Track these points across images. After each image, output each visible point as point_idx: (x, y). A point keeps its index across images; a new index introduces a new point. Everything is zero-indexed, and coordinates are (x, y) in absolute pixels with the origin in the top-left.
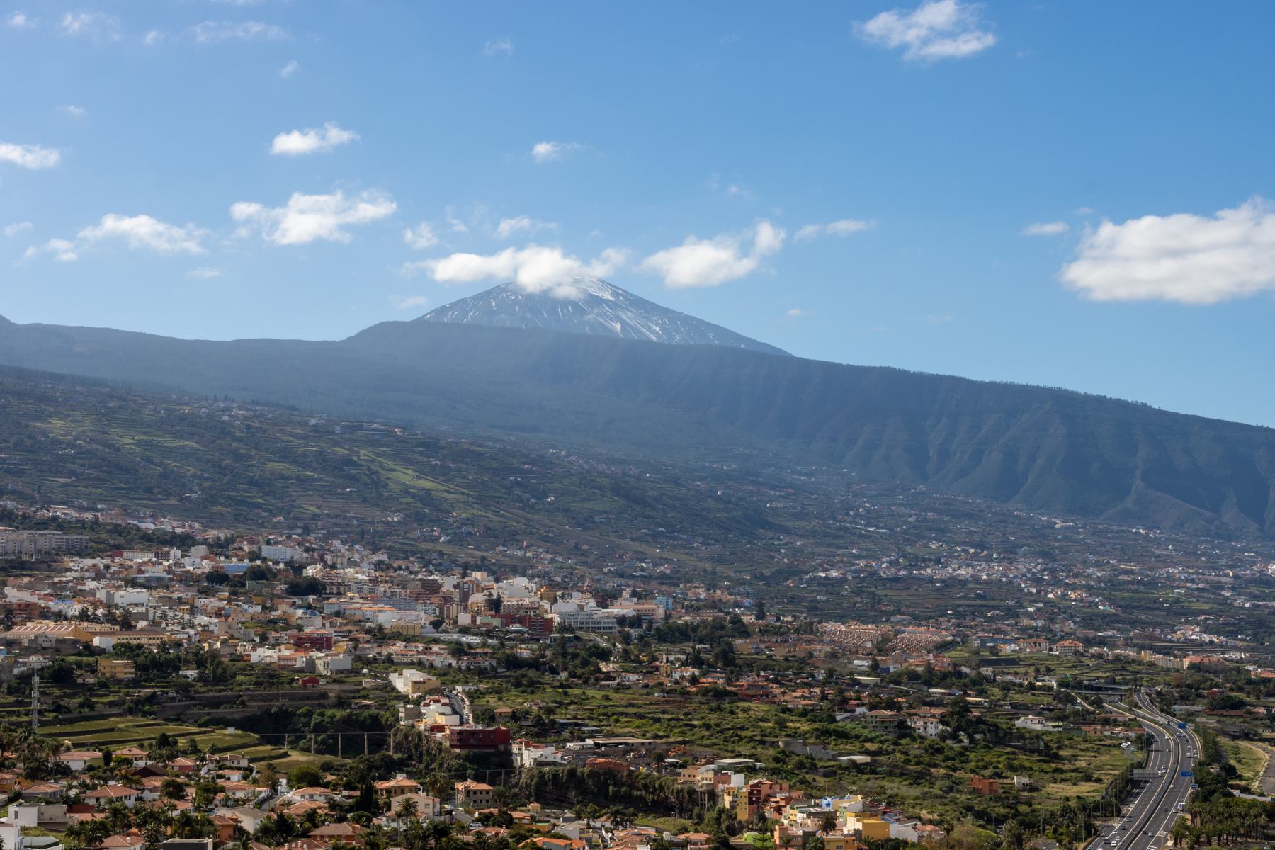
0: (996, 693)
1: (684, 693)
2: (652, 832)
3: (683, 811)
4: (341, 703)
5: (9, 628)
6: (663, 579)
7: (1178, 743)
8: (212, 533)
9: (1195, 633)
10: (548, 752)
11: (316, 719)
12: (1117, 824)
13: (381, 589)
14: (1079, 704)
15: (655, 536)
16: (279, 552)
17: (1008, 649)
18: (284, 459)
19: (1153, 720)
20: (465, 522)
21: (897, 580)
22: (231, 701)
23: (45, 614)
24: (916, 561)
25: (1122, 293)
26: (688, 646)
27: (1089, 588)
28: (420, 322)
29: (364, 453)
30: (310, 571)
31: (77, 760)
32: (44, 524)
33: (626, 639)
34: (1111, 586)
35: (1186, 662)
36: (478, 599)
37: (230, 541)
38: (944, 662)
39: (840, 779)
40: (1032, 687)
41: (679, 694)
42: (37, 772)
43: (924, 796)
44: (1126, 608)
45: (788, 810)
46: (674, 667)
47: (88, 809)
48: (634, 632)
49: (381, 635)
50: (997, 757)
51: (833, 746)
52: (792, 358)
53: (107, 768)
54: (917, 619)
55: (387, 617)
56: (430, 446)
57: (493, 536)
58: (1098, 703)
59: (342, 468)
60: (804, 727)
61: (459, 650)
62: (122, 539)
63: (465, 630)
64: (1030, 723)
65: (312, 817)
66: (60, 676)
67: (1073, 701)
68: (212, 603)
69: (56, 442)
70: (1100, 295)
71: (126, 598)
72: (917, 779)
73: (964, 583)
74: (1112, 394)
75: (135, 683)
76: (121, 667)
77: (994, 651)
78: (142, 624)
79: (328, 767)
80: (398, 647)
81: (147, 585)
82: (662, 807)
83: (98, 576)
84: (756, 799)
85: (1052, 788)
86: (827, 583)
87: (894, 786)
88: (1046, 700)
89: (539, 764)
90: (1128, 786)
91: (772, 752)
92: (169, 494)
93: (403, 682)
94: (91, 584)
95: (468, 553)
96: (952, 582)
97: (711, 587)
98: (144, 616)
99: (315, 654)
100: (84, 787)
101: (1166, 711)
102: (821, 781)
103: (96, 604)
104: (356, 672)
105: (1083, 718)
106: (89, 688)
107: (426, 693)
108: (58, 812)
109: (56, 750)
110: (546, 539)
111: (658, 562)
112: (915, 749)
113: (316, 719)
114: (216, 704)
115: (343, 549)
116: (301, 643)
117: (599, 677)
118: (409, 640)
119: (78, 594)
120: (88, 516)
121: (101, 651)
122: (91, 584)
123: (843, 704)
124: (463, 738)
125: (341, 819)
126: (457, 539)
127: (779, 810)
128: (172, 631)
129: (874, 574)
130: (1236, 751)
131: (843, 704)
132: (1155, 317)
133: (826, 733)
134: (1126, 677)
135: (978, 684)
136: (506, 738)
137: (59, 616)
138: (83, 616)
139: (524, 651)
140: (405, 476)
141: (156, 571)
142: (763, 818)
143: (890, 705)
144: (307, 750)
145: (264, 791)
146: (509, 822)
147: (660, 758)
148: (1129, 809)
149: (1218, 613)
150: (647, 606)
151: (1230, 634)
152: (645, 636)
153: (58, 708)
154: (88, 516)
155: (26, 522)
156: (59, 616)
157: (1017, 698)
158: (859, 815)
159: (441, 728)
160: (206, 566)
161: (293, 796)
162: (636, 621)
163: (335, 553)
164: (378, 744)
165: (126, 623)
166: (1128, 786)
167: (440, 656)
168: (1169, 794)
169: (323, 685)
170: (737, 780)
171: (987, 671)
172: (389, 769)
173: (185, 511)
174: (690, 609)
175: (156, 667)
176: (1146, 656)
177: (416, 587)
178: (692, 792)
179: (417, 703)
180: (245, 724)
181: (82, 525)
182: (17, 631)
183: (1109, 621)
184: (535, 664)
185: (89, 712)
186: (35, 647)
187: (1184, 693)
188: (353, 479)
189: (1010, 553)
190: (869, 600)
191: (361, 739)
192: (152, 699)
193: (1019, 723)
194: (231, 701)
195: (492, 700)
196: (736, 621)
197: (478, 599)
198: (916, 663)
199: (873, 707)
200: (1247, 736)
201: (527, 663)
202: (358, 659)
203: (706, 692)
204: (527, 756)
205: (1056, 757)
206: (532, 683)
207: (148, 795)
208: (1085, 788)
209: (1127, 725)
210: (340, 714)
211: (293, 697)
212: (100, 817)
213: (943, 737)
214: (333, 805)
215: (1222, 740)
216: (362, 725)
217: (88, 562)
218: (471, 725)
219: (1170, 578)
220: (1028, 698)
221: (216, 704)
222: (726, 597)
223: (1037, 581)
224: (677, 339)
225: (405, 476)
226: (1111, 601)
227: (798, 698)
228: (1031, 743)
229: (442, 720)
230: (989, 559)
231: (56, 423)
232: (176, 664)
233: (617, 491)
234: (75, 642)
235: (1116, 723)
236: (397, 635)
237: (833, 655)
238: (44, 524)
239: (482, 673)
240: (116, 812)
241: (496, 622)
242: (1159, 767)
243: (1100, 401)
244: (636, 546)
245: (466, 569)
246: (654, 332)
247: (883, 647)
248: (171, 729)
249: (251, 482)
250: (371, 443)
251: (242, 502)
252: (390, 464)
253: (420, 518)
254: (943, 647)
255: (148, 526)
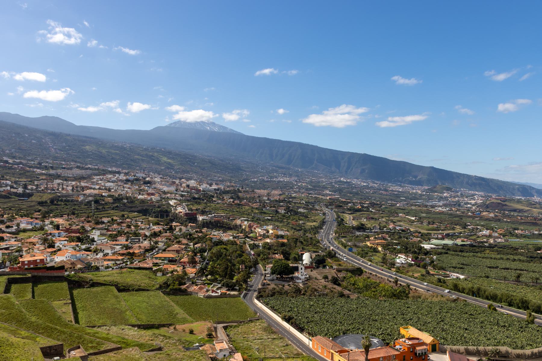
0: (293, 204)
1: (231, 204)
2: (231, 234)
3: (235, 229)
4: (159, 207)
5: (83, 191)
6: (220, 181)
7: (331, 215)
8: (124, 171)
9: (328, 192)
10: (205, 217)
11: (153, 211)
12: (322, 231)
13: (163, 183)
14: (310, 206)
15: (218, 172)
16: (140, 175)
17: (293, 195)
18: (138, 155)
19: (326, 210)
20: (178, 169)
21: (268, 181)
22: (135, 207)
23: (91, 188)
24: (271, 177)
25: (324, 124)
26: (230, 195)
27: (306, 183)
28: (166, 127)
29: (156, 154)
30: (147, 179)
31: (105, 220)
32: (87, 169)
33: (217, 193)
34: (311, 182)
35: (328, 198)
36: (184, 185)
37: (128, 172)
38: (282, 198)
39: (267, 222)
40: (300, 203)
41: (230, 205)
42: (97, 223)
43: (283, 226)
44: (314, 187)
45: (257, 229)
46: (228, 200)
47: (110, 231)
48: (218, 192)
49: (165, 193)
50: (296, 217)
51: (263, 215)
52: (245, 135)
53: (113, 221)
54: (273, 189)
55: (166, 189)
56: (170, 153)
57: (184, 172)
58: (314, 206)
59: (151, 157)
60: (257, 211)
61: (182, 196)
62: (105, 172)
63: (182, 192)
64: (301, 210)
65: (160, 232)
66: (96, 202)
67: (308, 206)
68: (127, 186)
69: (88, 151)
70: (317, 125)
71: (109, 185)
72: (281, 222)
73: (282, 182)
74: (310, 144)
75: (113, 203)
76: (110, 200)
77: (291, 196)
78: (113, 190)
79: (161, 221)
80: (169, 195)
81: (112, 182)
82: (230, 229)
83: (101, 180)
84: (250, 227)
85: (308, 223)
86: (254, 182)
87: (277, 224)
88: (303, 206)
89: (203, 220)
90: (323, 223)
91: (251, 217)
92: (113, 163)
93: (172, 202)
94: (100, 182)
95: (179, 175)
96: (279, 182)
97: (230, 182)
98: (113, 189)
99: (152, 197)
100: (109, 226)
101: (327, 207)
102: (262, 223)
103: (103, 186)
104: (161, 201)
105: (311, 209)
106: (103, 204)
107: (177, 205)
108: (104, 232)
109: (101, 218)
110: (195, 172)
111: (219, 177)
112: (280, 216)
113: (153, 211)
114: (131, 207)
115: (153, 174)
116: (148, 194)
117: (213, 202)
118: (171, 193)
119: (97, 184)
120: (97, 167)
121: (104, 196)
122: (100, 182)
123: (264, 207)
124: (186, 214)
125: (166, 232)
126: (176, 172)
127: (255, 229)
128: (120, 192)
129: (263, 180)
130: (343, 216)
131: (264, 207)
132: (330, 130)
133: (262, 213)
134: (318, 201)
135: (289, 202)
136: (196, 214)
137: (94, 189)
138: (99, 189)
139: (196, 196)
140: (165, 159)
141: (114, 179)
142: (251, 230)
143: (274, 207)
144: (152, 217)
145: (148, 226)
146: (202, 232)
147: (229, 218)
148: (324, 227)
149: (332, 188)
150: (220, 186)
151: (335, 192)
152: (221, 193)
153: (97, 209)
154: (97, 167)
155: (82, 168)
156: (94, 189)
157: (298, 205)
158: (272, 229)
159: (181, 212)
160: (125, 178)
161: (155, 227)
162: (218, 190)
163: (151, 175)
164: (167, 216)
165: (109, 190)
166: (323, 223)
167: (179, 198)
168: (331, 224)
169: (154, 203)
170: (246, 223)
171: (291, 200)
172: (172, 221)
173: (116, 166)
174: (228, 187)
175: (118, 200)
176: (320, 197)
177: (171, 182)
178: (236, 225)
179: (176, 207)
180: (139, 212)
181: (95, 169)
182: (85, 192)
183: (311, 189)
184: (199, 199)
185: (104, 209)
186: (90, 195)
187: (330, 204)
188: (154, 160)
189: (290, 176)
190: (263, 185)
191: (164, 214)
192: (117, 206)
193: (299, 210)
194: (135, 207)
195: (192, 206)
196: (238, 189)
197: (184, 185)
198: (277, 198)
199: (271, 207)
200: (343, 213)
201: (195, 198)
202: (161, 198)
203: (236, 204)
204: (200, 218)
205: (308, 217)
206: (199, 203)
207: (123, 228)
208: (314, 223)
209: (320, 211)
210: (159, 209)
211: (148, 206)
212: (114, 233)
213: (285, 213)
214: (164, 229)
215: (339, 213)
216: (164, 212)
217: (99, 177)
218: (188, 212)
219: (322, 181)
220: (299, 205)
221: (131, 207)
222: (234, 185)
223: (296, 181)
224: (221, 131)
225: (165, 159)
226: (311, 185)
227: (255, 205)
228: (302, 214)
229: (181, 211)
230: (286, 177)
231: (87, 147)
232: (122, 199)
233: (210, 162)
234: (99, 194)
235: (318, 210)
236: (168, 193)
237: (259, 197)
238: (87, 169)
239: (188, 201)
240: (119, 232)
241: (189, 190)
242: (328, 218)
243: (308, 145)
244: (214, 174)
245: (180, 179)
246: (216, 129)
247: (268, 195)
248: (123, 213)
249: (131, 160)
250: (157, 152)
251: (130, 164)
252: (161, 156)
253: (168, 168)
254: (280, 195)
255: (110, 169)
